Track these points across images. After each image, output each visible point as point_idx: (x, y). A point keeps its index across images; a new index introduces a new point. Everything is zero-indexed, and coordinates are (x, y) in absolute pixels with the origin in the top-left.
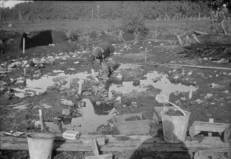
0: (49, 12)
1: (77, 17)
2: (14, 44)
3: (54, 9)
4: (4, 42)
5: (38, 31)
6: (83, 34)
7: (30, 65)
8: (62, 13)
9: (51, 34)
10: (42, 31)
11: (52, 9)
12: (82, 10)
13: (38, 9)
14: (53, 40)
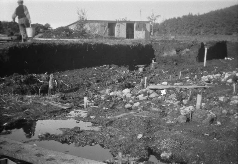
0: (198, 28)
3: (204, 24)
4: (178, 52)
5: (214, 42)
7: (232, 80)
8: (212, 29)
9: (226, 46)
11: (202, 24)
12: (235, 25)
13: (188, 25)
14: (228, 52)
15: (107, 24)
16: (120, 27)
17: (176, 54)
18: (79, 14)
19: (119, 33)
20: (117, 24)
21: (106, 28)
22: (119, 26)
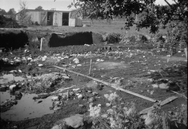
1: (48, 90)
2: (45, 42)
4: (40, 40)
5: (74, 33)
6: (125, 37)
10: (79, 32)
15: (47, 13)
16: (57, 15)
17: (38, 40)
18: (21, 5)
19: (56, 19)
20: (55, 13)
21: (45, 15)
22: (56, 14)
